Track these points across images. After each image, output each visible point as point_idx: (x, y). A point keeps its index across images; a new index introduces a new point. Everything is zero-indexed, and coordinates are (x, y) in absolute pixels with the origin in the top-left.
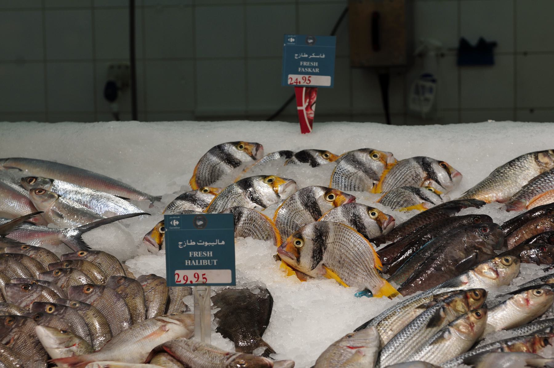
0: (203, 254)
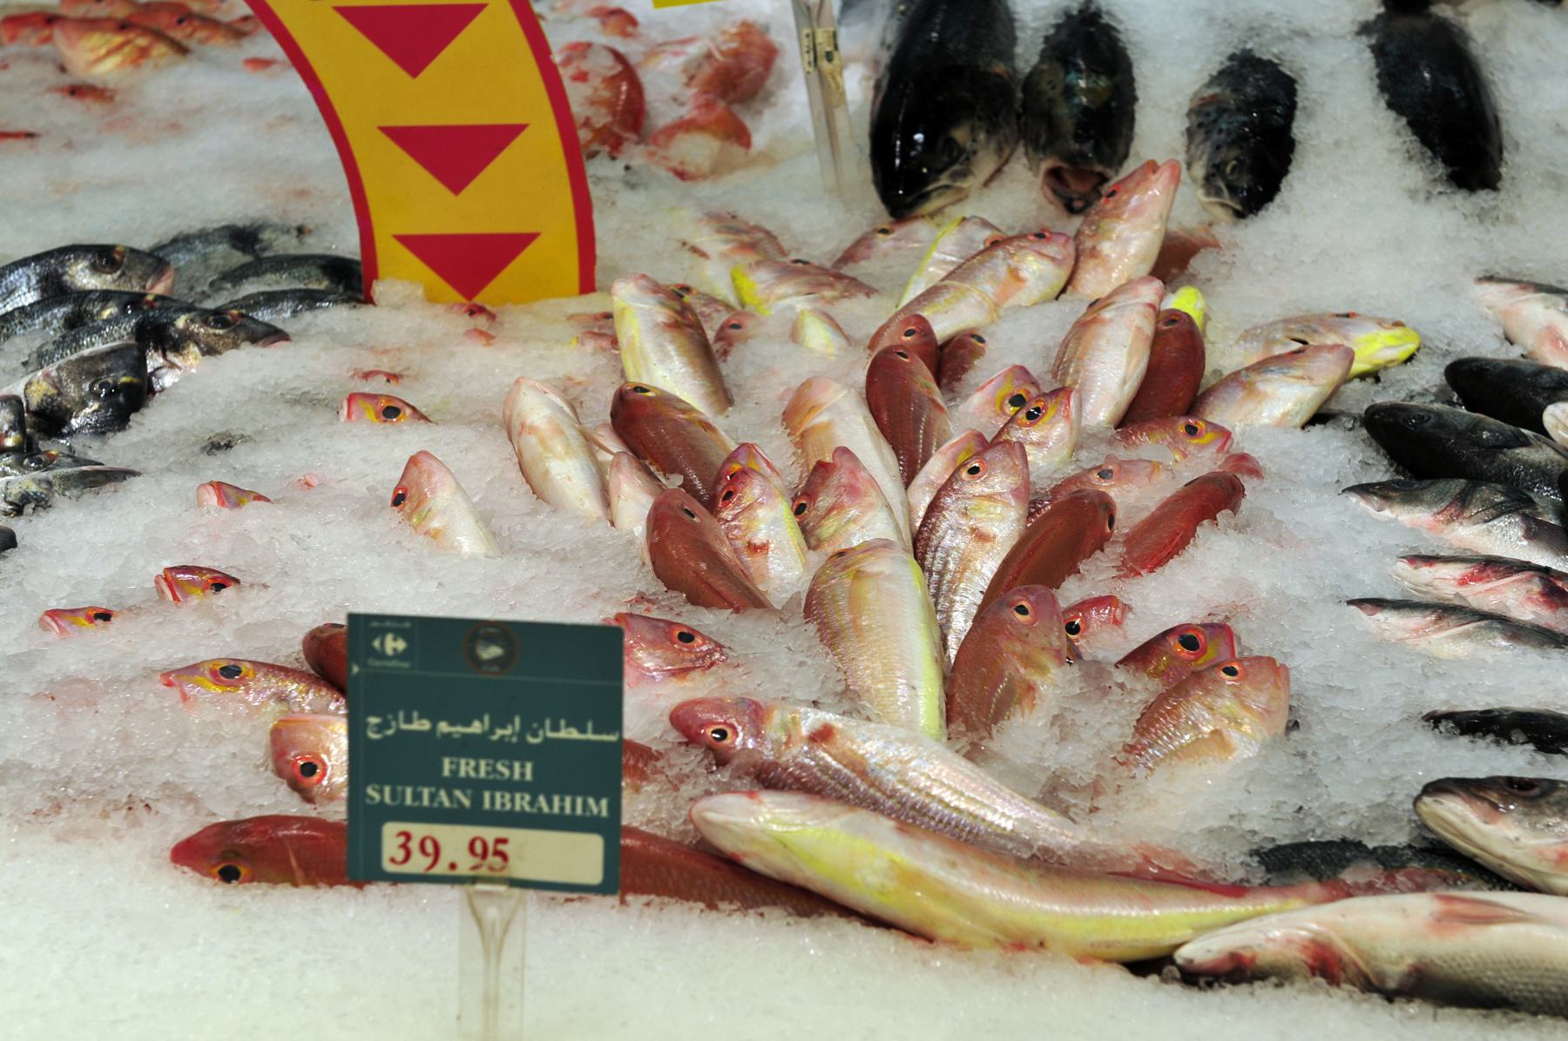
0: (495, 770)
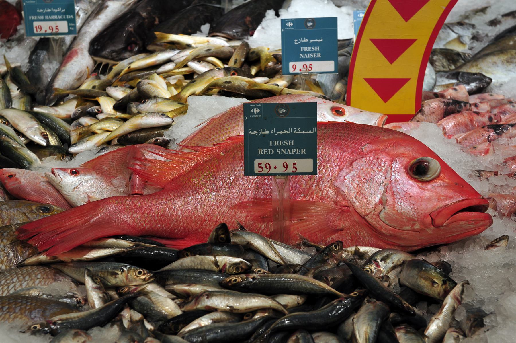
0: (284, 143)
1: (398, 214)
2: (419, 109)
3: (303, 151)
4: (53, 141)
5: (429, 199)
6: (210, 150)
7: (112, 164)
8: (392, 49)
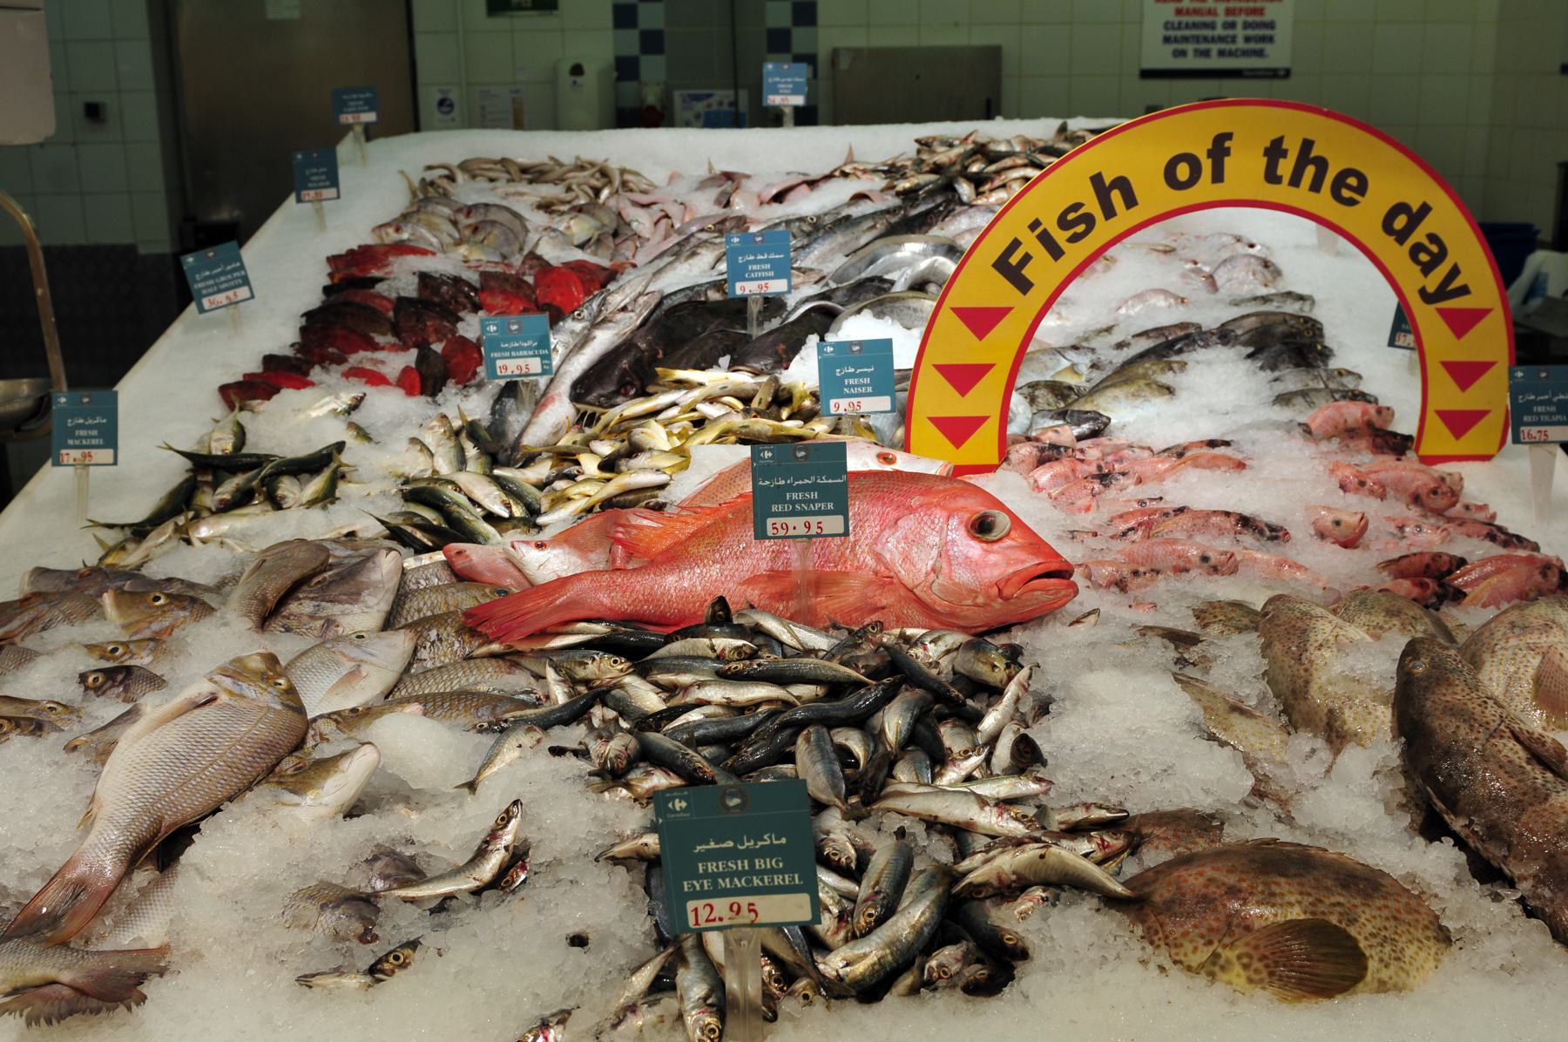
1: (955, 584)
2: (1004, 456)
3: (830, 506)
4: (518, 511)
5: (995, 565)
6: (716, 510)
7: (590, 535)
8: (963, 377)
